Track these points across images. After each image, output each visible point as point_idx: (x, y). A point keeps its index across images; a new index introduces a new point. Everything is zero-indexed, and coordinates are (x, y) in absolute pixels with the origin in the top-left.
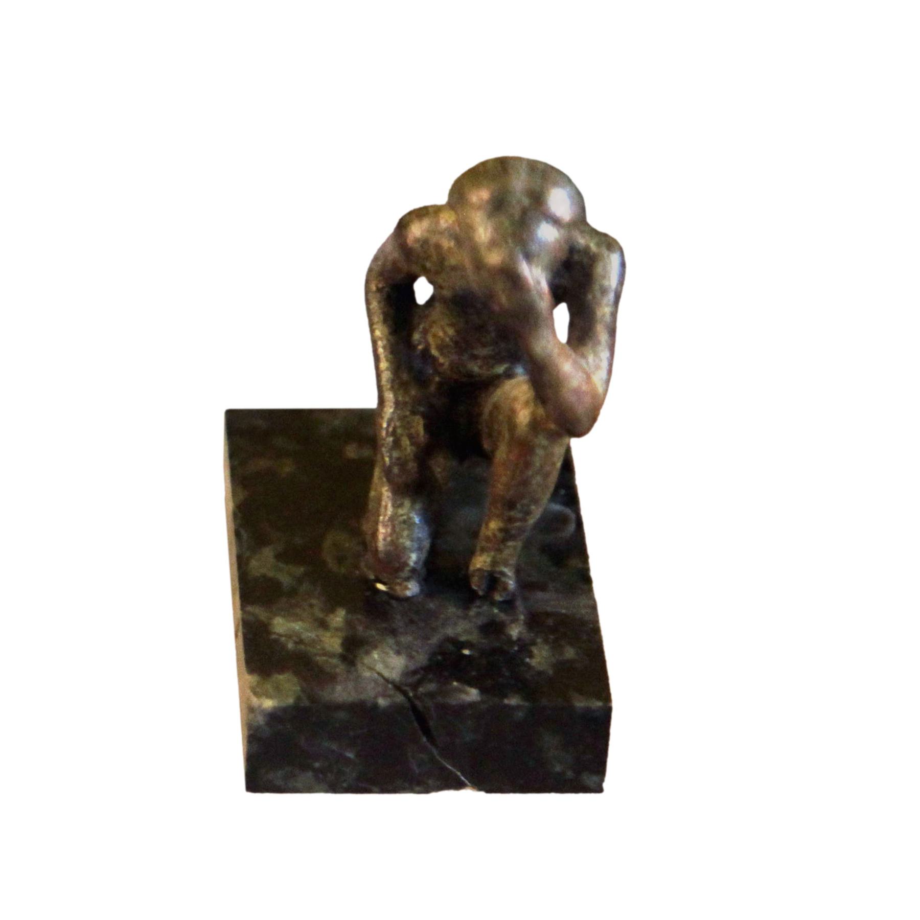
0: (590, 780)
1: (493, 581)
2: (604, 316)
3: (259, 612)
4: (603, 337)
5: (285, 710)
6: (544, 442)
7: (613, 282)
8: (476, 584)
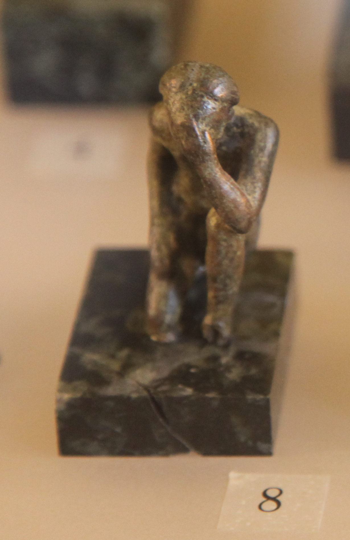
0: (262, 446)
1: (216, 332)
2: (260, 162)
3: (77, 350)
4: (259, 175)
5: (75, 400)
6: (225, 237)
7: (269, 145)
8: (207, 333)
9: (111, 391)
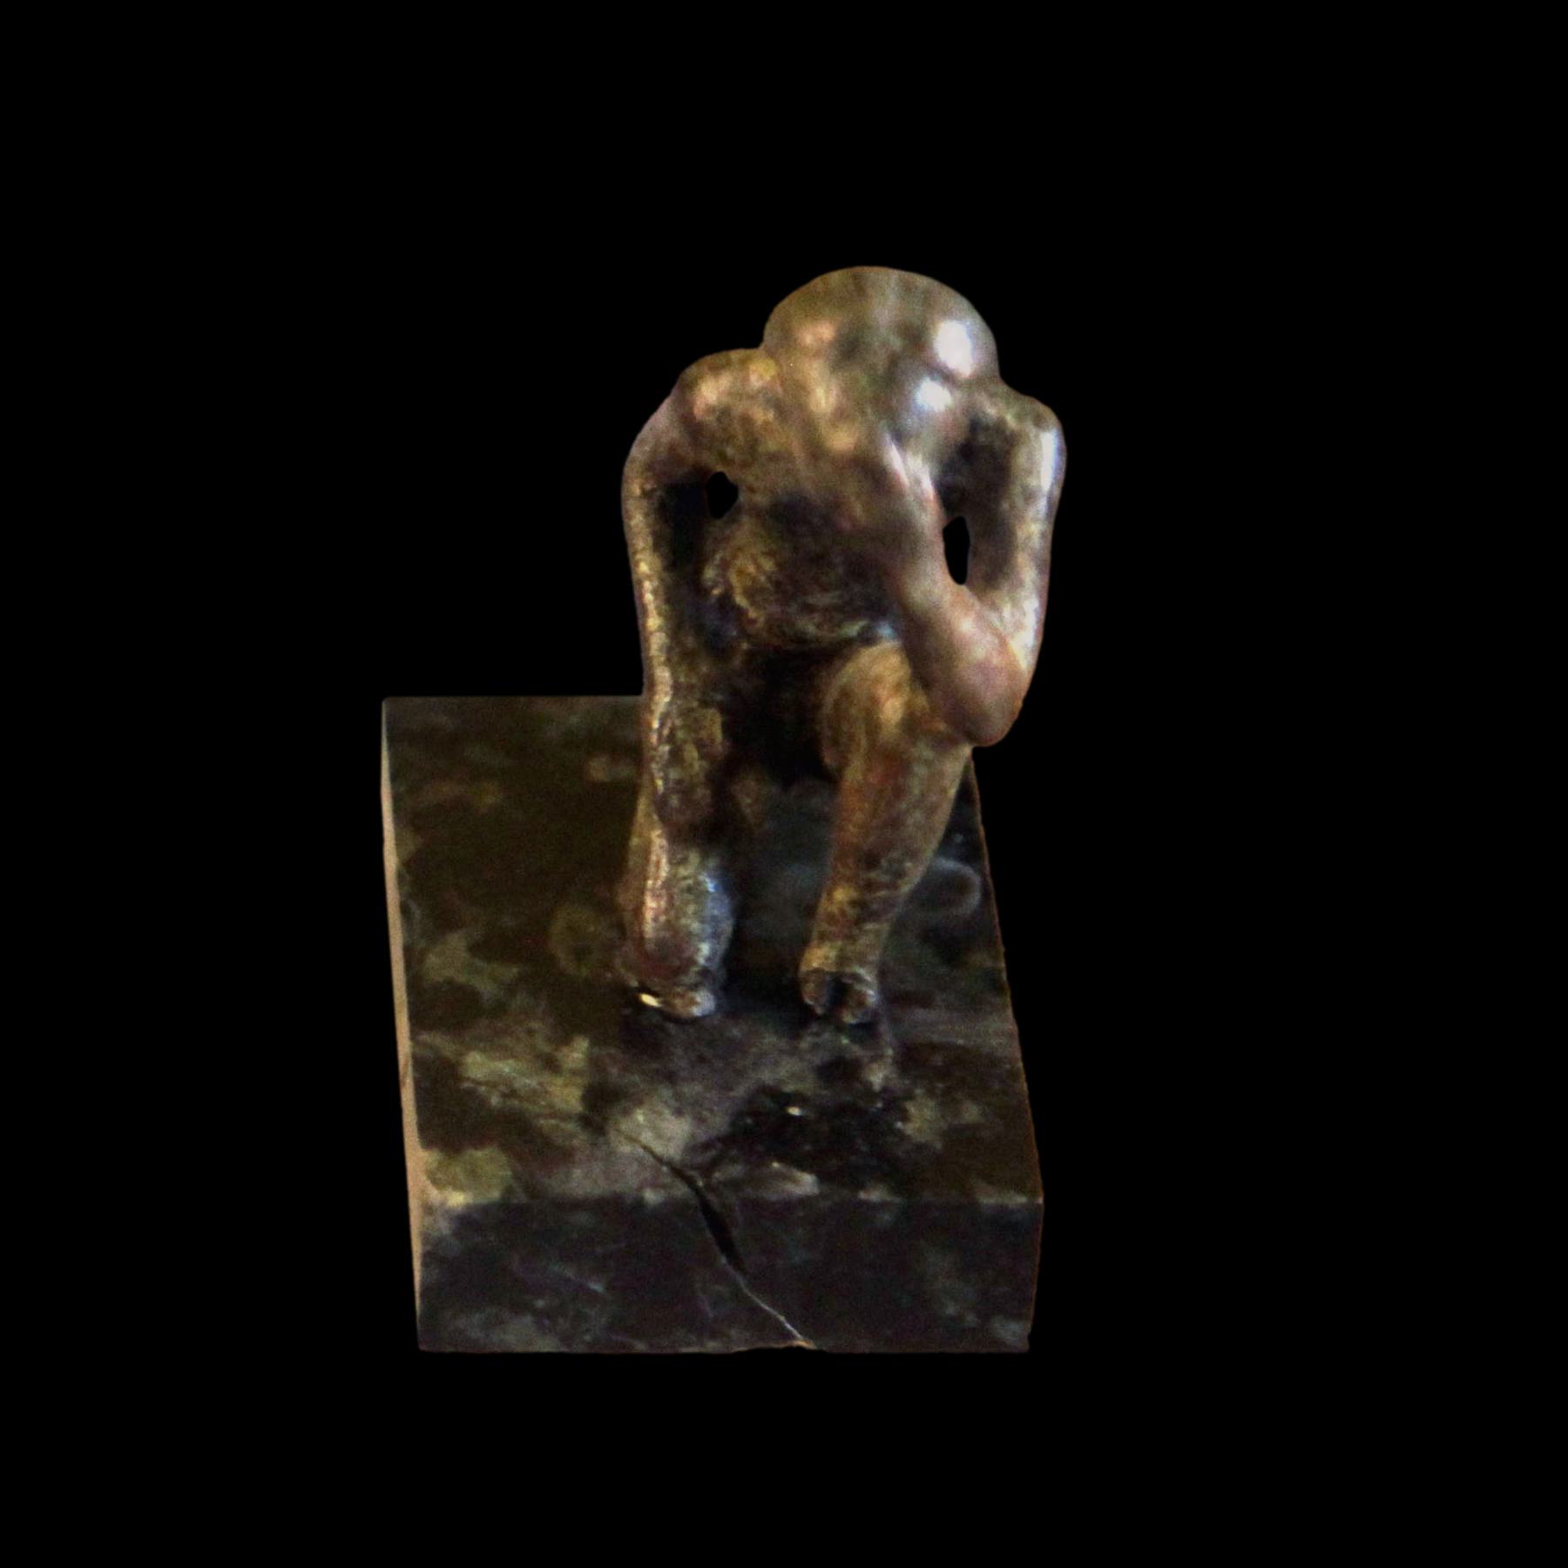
1: (841, 989)
2: (1029, 538)
5: (485, 1210)
6: (928, 754)
8: (812, 996)
9: (582, 1181)
